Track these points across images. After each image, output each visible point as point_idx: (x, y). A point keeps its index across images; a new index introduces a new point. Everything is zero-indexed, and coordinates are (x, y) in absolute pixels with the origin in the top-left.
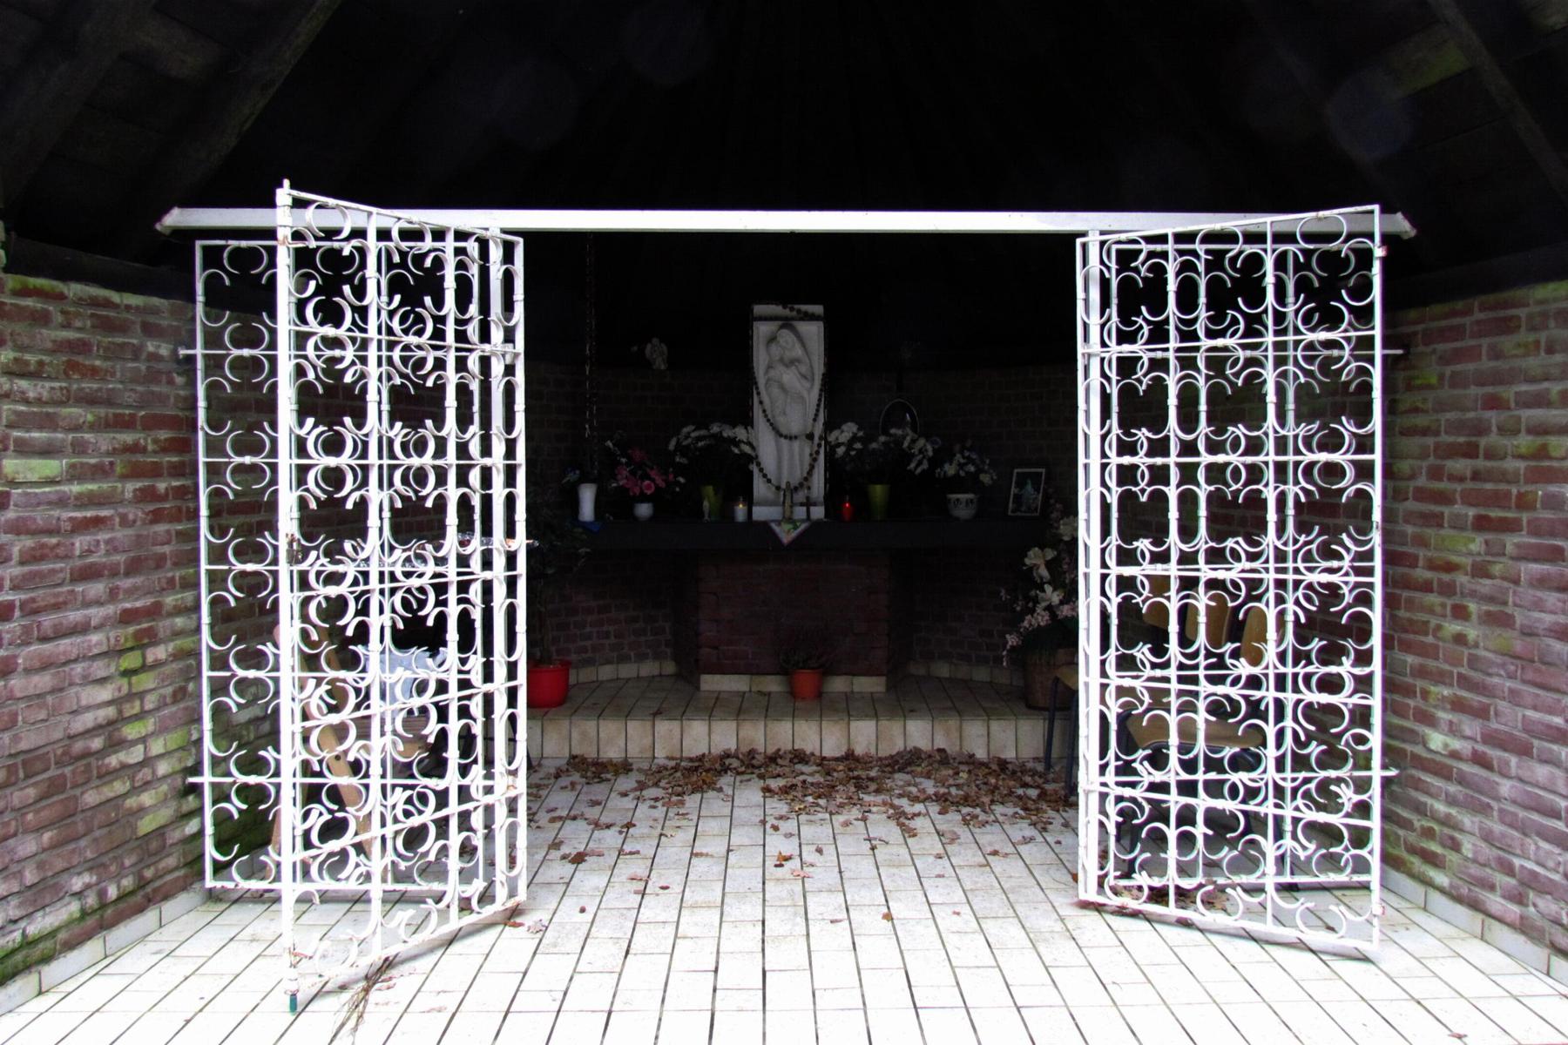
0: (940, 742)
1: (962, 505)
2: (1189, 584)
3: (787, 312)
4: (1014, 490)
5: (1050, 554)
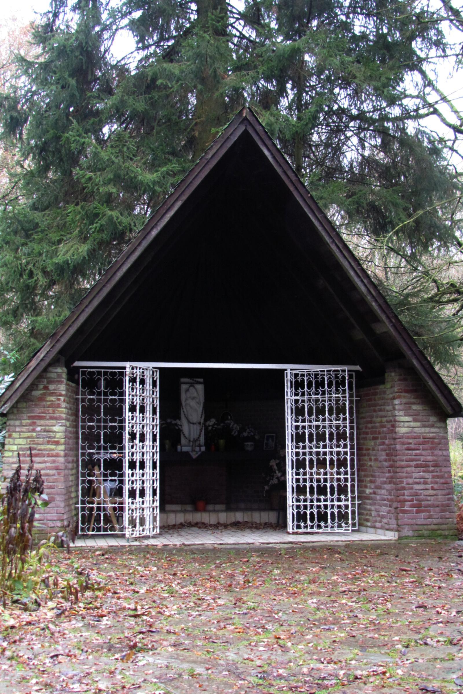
0: (246, 520)
1: (249, 446)
2: (332, 506)
3: (191, 381)
4: (265, 441)
5: (278, 461)
